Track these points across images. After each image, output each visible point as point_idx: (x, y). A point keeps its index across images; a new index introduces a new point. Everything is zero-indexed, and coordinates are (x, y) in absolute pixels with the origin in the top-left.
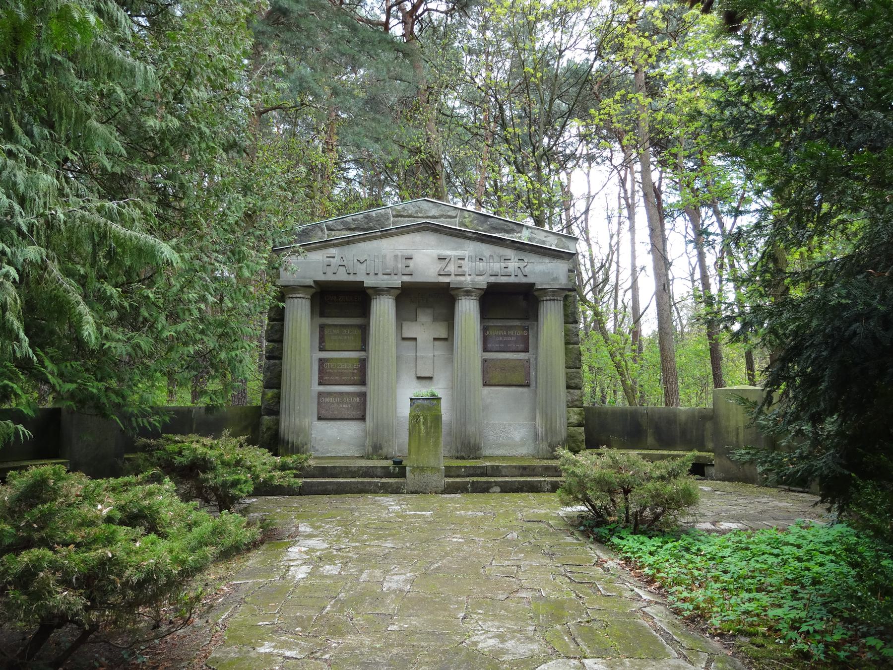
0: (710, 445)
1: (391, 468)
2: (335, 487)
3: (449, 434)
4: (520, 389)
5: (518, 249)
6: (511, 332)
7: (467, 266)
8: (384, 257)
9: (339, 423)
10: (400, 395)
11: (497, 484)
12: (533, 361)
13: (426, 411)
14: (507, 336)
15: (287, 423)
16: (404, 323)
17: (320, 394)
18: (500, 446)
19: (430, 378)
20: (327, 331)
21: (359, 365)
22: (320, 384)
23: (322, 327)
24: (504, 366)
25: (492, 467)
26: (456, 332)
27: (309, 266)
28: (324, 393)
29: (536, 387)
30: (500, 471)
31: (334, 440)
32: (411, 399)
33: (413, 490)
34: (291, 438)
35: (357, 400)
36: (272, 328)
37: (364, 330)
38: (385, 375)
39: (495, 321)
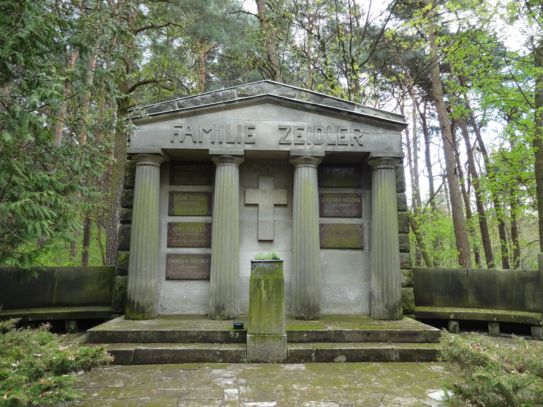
0: (531, 306)
1: (232, 333)
2: (172, 356)
3: (290, 293)
4: (354, 252)
5: (354, 120)
6: (345, 200)
7: (306, 136)
8: (229, 127)
9: (185, 283)
10: (243, 256)
11: (342, 352)
12: (366, 226)
13: (267, 273)
14: (342, 202)
15: (133, 284)
16: (247, 190)
17: (169, 256)
18: (336, 305)
19: (271, 241)
20: (176, 198)
21: (205, 229)
22: (169, 246)
23: (172, 194)
24: (338, 230)
25: (335, 332)
26: (295, 198)
27: (155, 136)
28: (172, 255)
29: (370, 250)
30: (343, 337)
31: (180, 299)
32: (252, 262)
33: (254, 358)
34: (136, 298)
35: (202, 261)
36: (126, 195)
37: (210, 197)
38: (228, 238)
39: (330, 189)
